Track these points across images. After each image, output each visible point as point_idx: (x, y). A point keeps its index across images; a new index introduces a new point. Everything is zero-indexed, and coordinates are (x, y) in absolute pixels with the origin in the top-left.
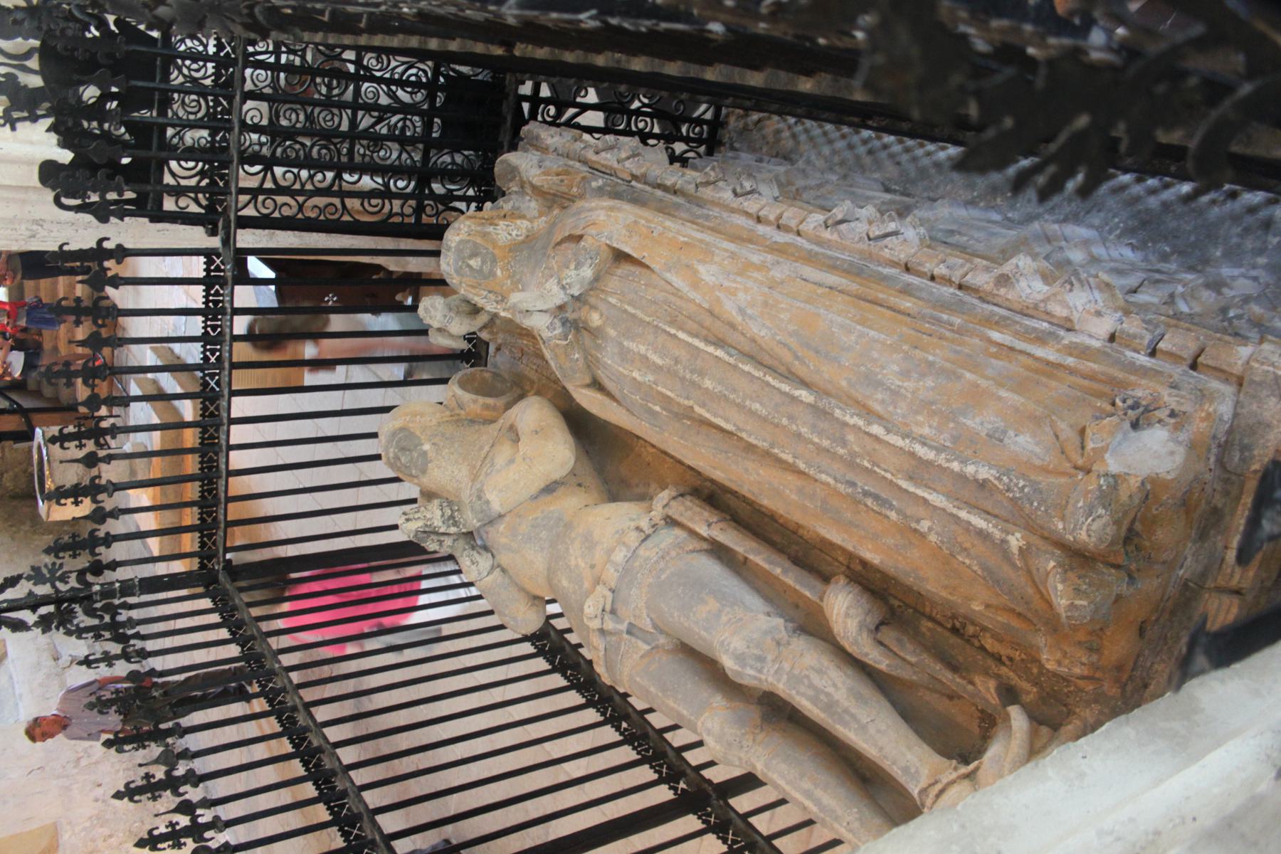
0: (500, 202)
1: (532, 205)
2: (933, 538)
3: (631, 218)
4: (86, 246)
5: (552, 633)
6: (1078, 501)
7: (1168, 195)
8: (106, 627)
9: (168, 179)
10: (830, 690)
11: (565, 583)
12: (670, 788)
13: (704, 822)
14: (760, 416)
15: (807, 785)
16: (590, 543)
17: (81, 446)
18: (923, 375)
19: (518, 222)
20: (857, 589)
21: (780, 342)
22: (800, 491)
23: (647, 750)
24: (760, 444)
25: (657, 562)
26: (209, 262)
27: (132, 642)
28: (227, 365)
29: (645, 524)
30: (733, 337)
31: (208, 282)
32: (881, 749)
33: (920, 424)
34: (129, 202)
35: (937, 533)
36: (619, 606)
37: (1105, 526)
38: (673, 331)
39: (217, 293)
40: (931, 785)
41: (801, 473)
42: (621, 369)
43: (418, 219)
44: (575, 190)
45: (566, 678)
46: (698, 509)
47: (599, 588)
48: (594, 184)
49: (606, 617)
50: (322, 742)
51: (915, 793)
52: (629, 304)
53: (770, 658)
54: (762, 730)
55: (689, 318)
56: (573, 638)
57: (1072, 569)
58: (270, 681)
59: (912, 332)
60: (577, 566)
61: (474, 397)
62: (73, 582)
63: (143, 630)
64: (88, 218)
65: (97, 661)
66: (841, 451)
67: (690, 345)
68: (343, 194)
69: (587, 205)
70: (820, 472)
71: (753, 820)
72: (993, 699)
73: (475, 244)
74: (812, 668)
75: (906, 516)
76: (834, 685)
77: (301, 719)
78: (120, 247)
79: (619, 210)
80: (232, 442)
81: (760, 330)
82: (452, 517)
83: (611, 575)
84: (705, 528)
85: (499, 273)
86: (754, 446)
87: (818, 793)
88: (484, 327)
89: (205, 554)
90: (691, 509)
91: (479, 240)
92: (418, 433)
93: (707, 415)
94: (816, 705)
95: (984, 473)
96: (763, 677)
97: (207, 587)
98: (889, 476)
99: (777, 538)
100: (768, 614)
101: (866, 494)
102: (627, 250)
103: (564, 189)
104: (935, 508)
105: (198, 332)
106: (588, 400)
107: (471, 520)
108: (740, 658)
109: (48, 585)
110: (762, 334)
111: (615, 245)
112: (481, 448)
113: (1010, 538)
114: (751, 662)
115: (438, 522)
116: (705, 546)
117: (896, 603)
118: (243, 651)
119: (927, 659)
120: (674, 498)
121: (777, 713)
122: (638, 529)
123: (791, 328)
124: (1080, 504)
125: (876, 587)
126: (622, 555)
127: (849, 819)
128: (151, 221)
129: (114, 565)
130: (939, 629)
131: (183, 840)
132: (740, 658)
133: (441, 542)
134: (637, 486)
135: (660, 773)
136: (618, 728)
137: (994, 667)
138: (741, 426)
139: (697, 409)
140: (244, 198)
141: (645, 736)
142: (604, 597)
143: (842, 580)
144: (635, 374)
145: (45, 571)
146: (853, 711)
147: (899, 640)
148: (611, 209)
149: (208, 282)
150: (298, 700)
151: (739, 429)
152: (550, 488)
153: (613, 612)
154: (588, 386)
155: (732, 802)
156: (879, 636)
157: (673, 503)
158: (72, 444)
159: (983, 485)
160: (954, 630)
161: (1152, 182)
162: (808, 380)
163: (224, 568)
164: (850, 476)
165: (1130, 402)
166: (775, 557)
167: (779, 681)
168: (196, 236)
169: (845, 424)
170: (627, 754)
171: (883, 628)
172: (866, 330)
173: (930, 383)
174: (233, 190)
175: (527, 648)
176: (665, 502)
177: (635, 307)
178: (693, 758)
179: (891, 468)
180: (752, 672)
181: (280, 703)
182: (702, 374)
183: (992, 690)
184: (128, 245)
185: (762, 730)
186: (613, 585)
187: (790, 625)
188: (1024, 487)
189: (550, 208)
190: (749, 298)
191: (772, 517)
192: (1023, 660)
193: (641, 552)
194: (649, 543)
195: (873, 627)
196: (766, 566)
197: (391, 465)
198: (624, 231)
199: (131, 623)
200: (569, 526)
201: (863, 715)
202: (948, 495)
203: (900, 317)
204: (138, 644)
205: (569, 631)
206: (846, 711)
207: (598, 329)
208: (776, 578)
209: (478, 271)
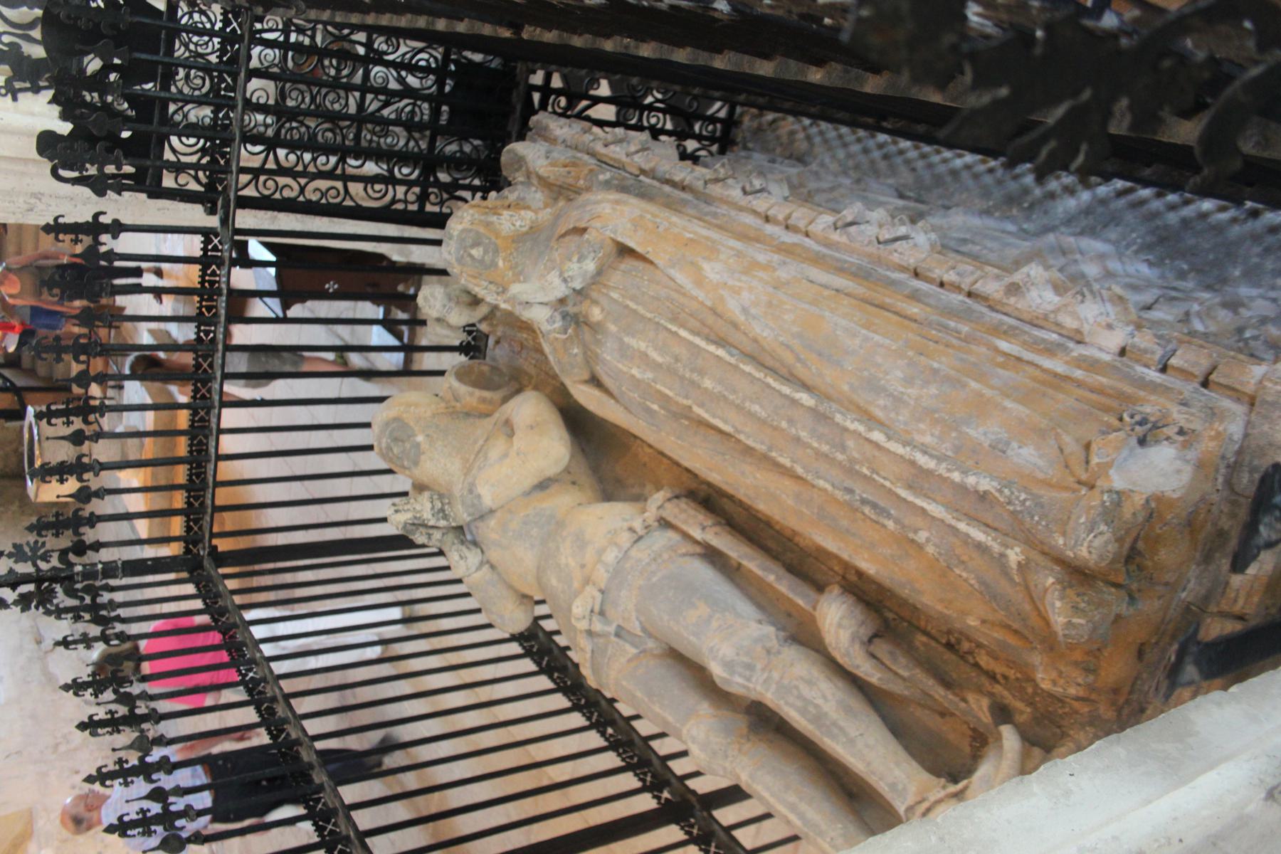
0: (506, 192)
1: (537, 196)
2: (930, 549)
3: (637, 212)
4: (81, 220)
5: (541, 635)
6: (1079, 517)
7: (1188, 211)
8: (87, 608)
9: (168, 155)
10: (820, 701)
11: (554, 582)
12: (654, 797)
14: (759, 419)
15: (792, 798)
16: (581, 543)
17: (69, 423)
18: (927, 383)
19: (523, 212)
20: (850, 600)
21: (782, 344)
23: (631, 758)
24: (758, 446)
25: (648, 564)
26: (207, 242)
29: (638, 525)
30: (735, 337)
32: (869, 764)
33: (923, 433)
35: (935, 545)
37: (1107, 543)
38: (674, 328)
39: (214, 273)
41: (799, 478)
42: (620, 366)
44: (582, 182)
47: (588, 588)
48: (601, 177)
50: (300, 734)
52: (631, 300)
53: (759, 666)
55: (691, 315)
59: (919, 338)
60: (567, 565)
61: (470, 389)
63: (123, 612)
65: (75, 642)
66: (840, 457)
67: (691, 343)
68: (346, 178)
70: (819, 478)
72: (986, 718)
73: (477, 233)
74: (802, 678)
75: (903, 526)
76: (824, 697)
77: (281, 710)
79: (625, 203)
80: (224, 425)
81: (762, 331)
82: (442, 510)
83: (602, 576)
84: (699, 531)
85: (501, 263)
86: (752, 449)
87: (803, 807)
89: (191, 539)
90: (685, 511)
91: (482, 230)
92: (412, 424)
93: (706, 416)
95: (985, 484)
96: (751, 685)
97: (191, 572)
98: (887, 484)
99: (771, 544)
100: (760, 622)
101: (864, 502)
103: (570, 181)
104: (933, 518)
105: (191, 311)
106: (586, 396)
107: (461, 515)
108: (729, 665)
110: (765, 334)
111: (620, 239)
112: (475, 442)
113: (1009, 552)
114: (740, 670)
115: (427, 515)
116: (698, 550)
119: (919, 674)
120: (669, 500)
122: (631, 530)
123: (795, 329)
124: (1082, 520)
126: (613, 555)
128: (149, 197)
130: (934, 644)
131: (153, 828)
132: (729, 665)
133: (429, 536)
134: (633, 486)
136: (603, 734)
139: (696, 409)
140: (244, 178)
142: (593, 598)
143: (836, 590)
144: (635, 371)
145: (27, 549)
147: (891, 653)
148: (617, 202)
150: (277, 690)
152: (543, 485)
153: (602, 613)
154: (586, 382)
155: (717, 814)
156: (872, 648)
157: (668, 505)
158: (58, 421)
159: (983, 497)
160: (950, 646)
161: (1172, 198)
162: (810, 383)
163: (209, 554)
164: (849, 483)
165: (1137, 418)
166: (769, 563)
167: (767, 690)
168: (195, 215)
169: (846, 430)
170: (611, 760)
171: (876, 640)
172: (871, 335)
173: (933, 390)
174: (234, 168)
175: (515, 648)
177: (637, 303)
179: (891, 478)
180: (739, 680)
182: (702, 372)
183: (985, 709)
184: (124, 221)
186: (603, 586)
187: (782, 634)
188: (1025, 500)
189: (556, 200)
190: (753, 297)
191: (768, 523)
192: (1017, 679)
193: (633, 553)
194: (641, 544)
195: (865, 639)
197: (384, 456)
198: (629, 225)
199: (112, 605)
200: (560, 524)
202: (947, 506)
203: (906, 322)
206: (834, 724)
207: (599, 324)
208: (770, 585)
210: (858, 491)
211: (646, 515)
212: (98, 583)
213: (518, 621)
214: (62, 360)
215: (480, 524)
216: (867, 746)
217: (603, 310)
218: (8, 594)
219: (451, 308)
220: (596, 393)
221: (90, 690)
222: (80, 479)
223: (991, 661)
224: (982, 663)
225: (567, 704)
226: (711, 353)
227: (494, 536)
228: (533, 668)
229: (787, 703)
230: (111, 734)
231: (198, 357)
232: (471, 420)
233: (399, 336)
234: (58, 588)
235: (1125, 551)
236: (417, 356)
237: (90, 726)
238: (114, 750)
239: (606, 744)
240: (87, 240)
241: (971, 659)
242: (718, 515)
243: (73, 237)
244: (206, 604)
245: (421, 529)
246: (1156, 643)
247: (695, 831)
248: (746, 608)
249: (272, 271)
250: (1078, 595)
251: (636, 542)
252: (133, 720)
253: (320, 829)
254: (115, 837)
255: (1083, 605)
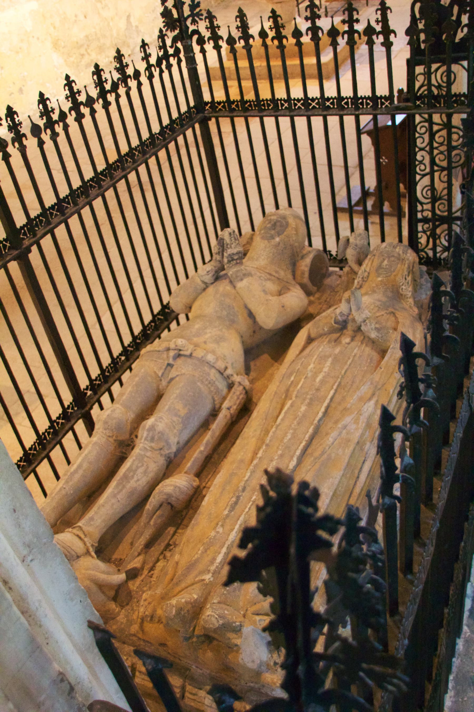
4: (390, 23)
6: (228, 611)
8: (166, 52)
10: (135, 478)
11: (197, 326)
12: (87, 386)
13: (69, 406)
14: (283, 438)
15: (85, 465)
17: (271, 28)
20: (191, 492)
22: (242, 461)
23: (109, 372)
25: (207, 380)
26: (386, 98)
27: (158, 69)
28: (325, 113)
29: (229, 371)
31: (374, 98)
34: (419, 45)
35: (215, 536)
36: (182, 358)
37: (213, 624)
40: (84, 532)
42: (315, 357)
43: (420, 221)
45: (150, 323)
46: (238, 402)
49: (176, 352)
50: (104, 188)
51: (80, 524)
54: (115, 440)
56: (173, 325)
57: (193, 607)
58: (139, 152)
60: (206, 333)
62: (192, 28)
63: (166, 75)
64: (408, 24)
65: (145, 51)
69: (418, 331)
70: (251, 473)
71: (70, 434)
72: (130, 566)
74: (148, 467)
75: (225, 519)
76: (138, 480)
77: (119, 173)
78: (391, 44)
80: (280, 118)
83: (199, 353)
87: (81, 472)
88: (352, 269)
90: (238, 398)
92: (285, 233)
94: (128, 469)
96: (143, 441)
97: (194, 107)
99: (222, 446)
100: (178, 443)
102: (386, 358)
105: (343, 94)
107: (231, 271)
108: (152, 428)
109: (189, 13)
111: (389, 351)
114: (151, 435)
115: (230, 251)
116: (217, 406)
117: (184, 513)
118: (156, 134)
120: (244, 388)
121: (123, 448)
122: (226, 368)
123: (333, 455)
124: (226, 612)
125: (193, 500)
127: (67, 488)
129: (203, 51)
130: (169, 537)
131: (45, 118)
135: (96, 380)
136: (121, 355)
137: (147, 567)
138: (279, 427)
140: (426, 116)
141: (116, 370)
144: (312, 366)
145: (198, 10)
146: (124, 491)
149: (374, 98)
150: (128, 170)
151: (278, 426)
152: (251, 315)
153: (179, 356)
155: (81, 421)
157: (241, 388)
160: (168, 545)
163: (205, 117)
166: (210, 446)
170: (106, 361)
171: (170, 506)
176: (242, 383)
178: (105, 399)
181: (127, 160)
183: (135, 566)
184: (393, 48)
185: (115, 440)
186: (194, 355)
187: (172, 456)
190: (352, 431)
192: (151, 582)
193: (213, 371)
194: (218, 375)
195: (169, 501)
196: (205, 441)
199: (169, 67)
201: (122, 496)
204: (156, 73)
205: (178, 324)
206: (124, 487)
207: (340, 343)
209: (380, 265)
210: (244, 494)
211: (235, 376)
212: (182, 55)
213: (176, 304)
214: (307, 21)
215: (228, 281)
216: (113, 504)
217: (349, 344)
218: (170, 3)
219: (356, 249)
220: (303, 343)
221: (118, 66)
222: (240, 38)
223: (161, 568)
224: (159, 564)
225: (136, 333)
226: (320, 409)
227: (221, 289)
228: (156, 312)
229: (134, 460)
230: (95, 82)
231: (318, 99)
232: (291, 268)
233: (357, 204)
234: (177, 32)
235: (212, 634)
236: (347, 216)
237: (98, 71)
238: (85, 87)
239: (115, 356)
240: (378, 28)
241: (161, 557)
242: (238, 416)
243: (380, 19)
244: (176, 119)
245: (221, 249)
246: (169, 653)
247: (70, 411)
248: (185, 436)
249: (390, 123)
250: (188, 611)
251: (220, 372)
252: (103, 94)
253: (52, 207)
254: (38, 98)
255: (183, 613)
